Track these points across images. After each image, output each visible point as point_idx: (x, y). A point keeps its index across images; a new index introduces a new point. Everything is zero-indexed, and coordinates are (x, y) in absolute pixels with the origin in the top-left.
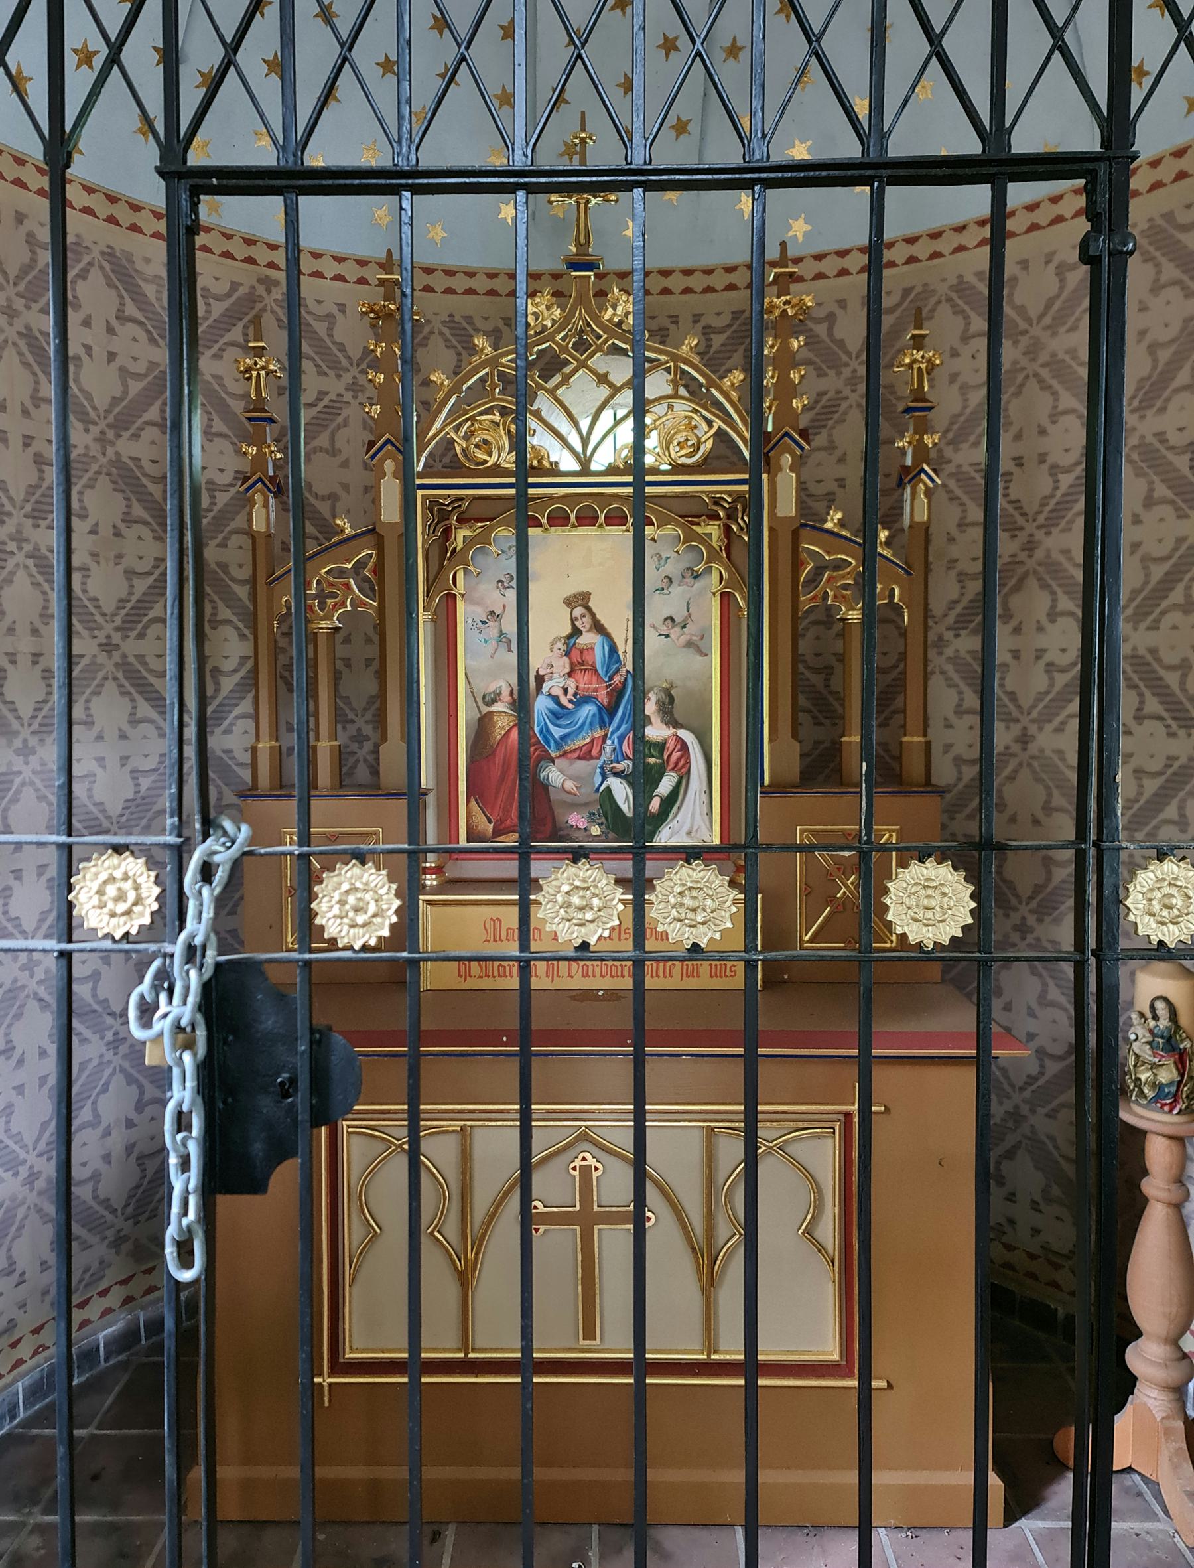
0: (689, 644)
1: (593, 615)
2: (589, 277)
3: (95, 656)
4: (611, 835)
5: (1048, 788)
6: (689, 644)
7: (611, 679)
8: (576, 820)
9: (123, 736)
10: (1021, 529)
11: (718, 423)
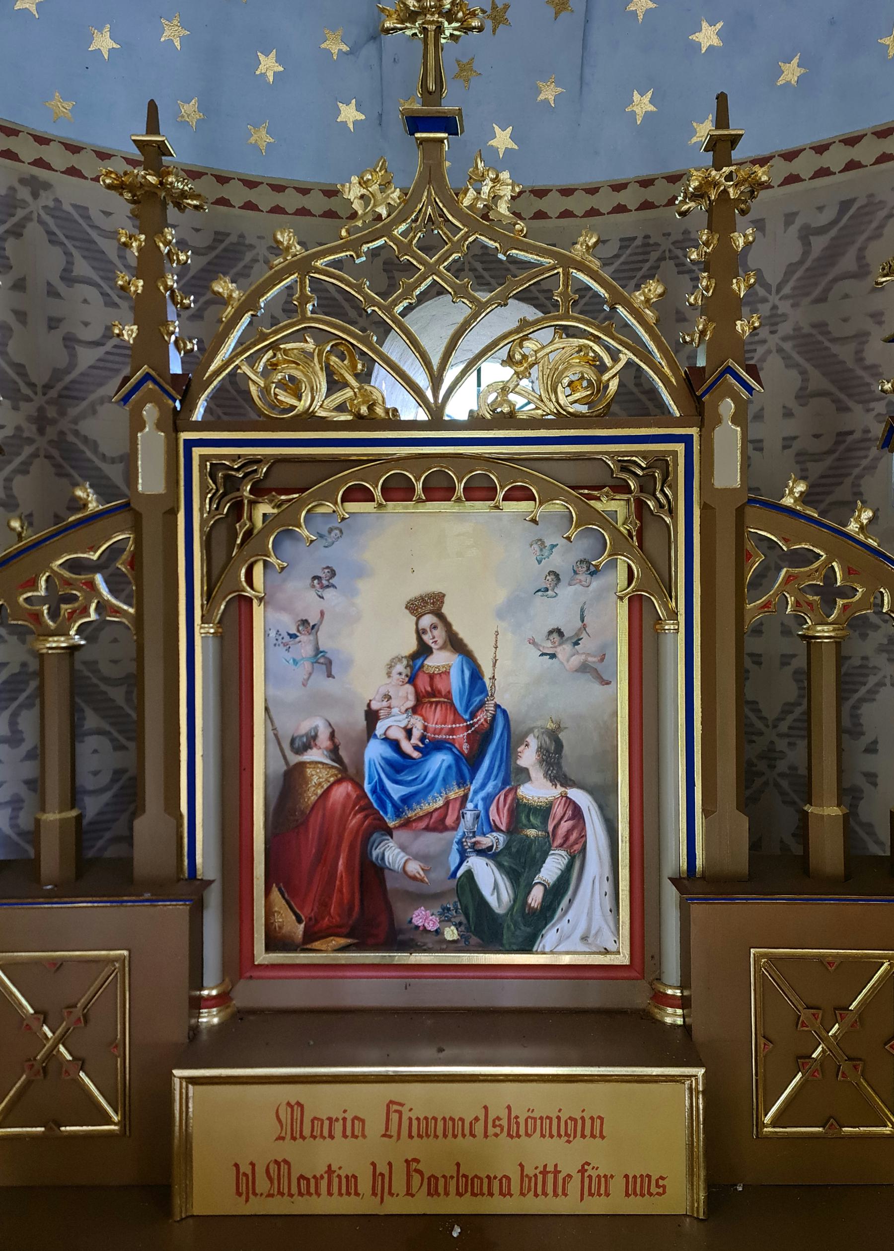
0: (584, 668)
1: (448, 626)
2: (441, 141)
4: (474, 940)
6: (584, 668)
7: (473, 715)
11: (626, 356)
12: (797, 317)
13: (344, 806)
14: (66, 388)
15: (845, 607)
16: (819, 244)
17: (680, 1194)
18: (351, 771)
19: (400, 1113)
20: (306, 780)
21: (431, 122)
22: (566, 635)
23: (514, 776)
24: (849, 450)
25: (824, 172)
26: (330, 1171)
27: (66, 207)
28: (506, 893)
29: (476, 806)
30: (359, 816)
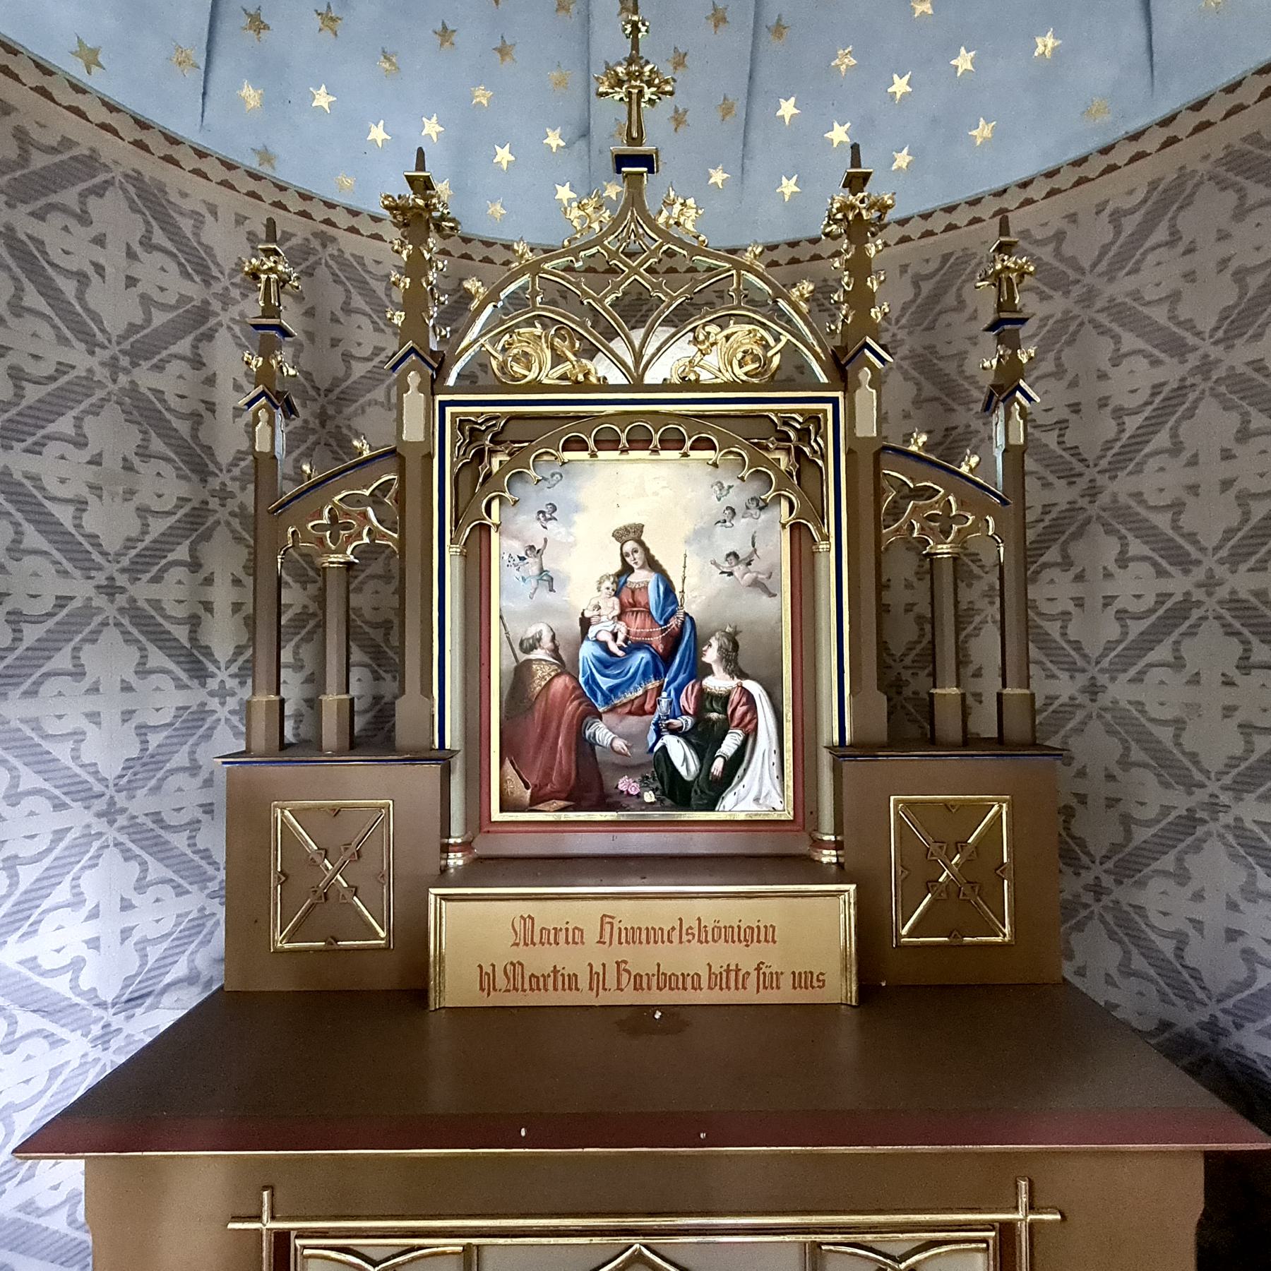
0: (756, 584)
1: (646, 550)
2: (641, 174)
3: (90, 599)
4: (668, 802)
5: (1124, 741)
6: (756, 584)
7: (666, 622)
8: (627, 784)
9: (126, 688)
10: (1080, 475)
11: (786, 337)
12: (910, 343)
13: (563, 696)
14: (342, 392)
15: (959, 530)
16: (926, 287)
17: (840, 988)
18: (569, 667)
19: (612, 924)
20: (532, 675)
21: (634, 161)
22: (741, 557)
23: (700, 671)
24: (954, 441)
25: (929, 233)
26: (555, 971)
27: (347, 256)
28: (694, 765)
29: (669, 695)
30: (576, 703)
